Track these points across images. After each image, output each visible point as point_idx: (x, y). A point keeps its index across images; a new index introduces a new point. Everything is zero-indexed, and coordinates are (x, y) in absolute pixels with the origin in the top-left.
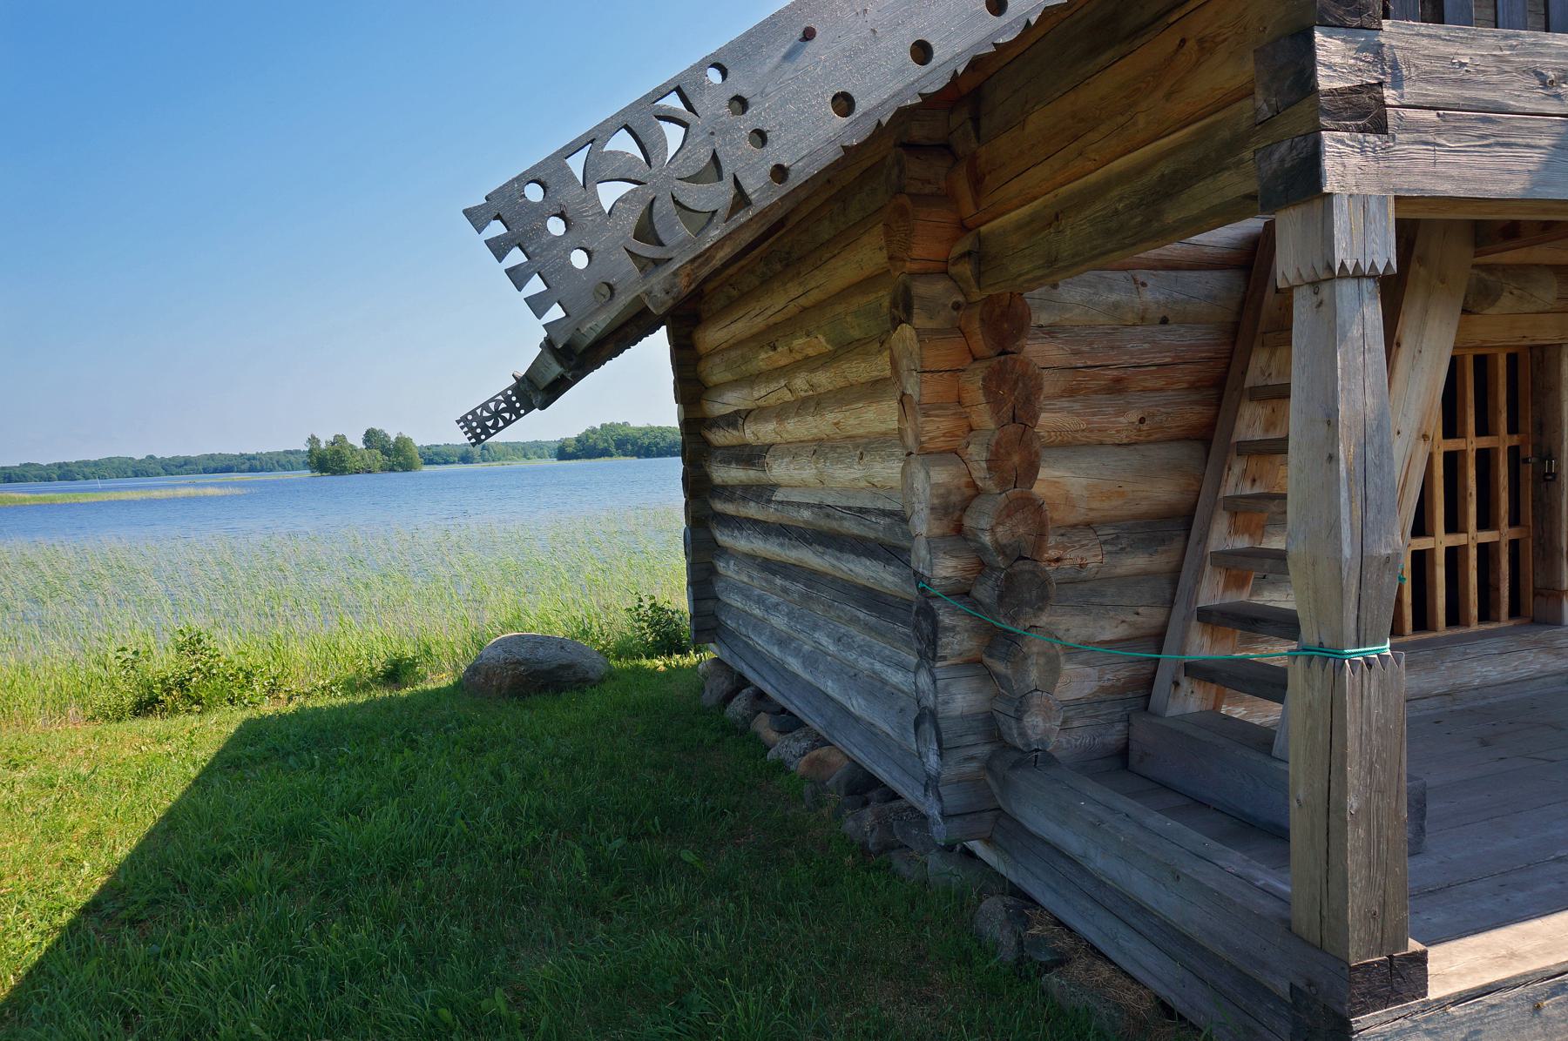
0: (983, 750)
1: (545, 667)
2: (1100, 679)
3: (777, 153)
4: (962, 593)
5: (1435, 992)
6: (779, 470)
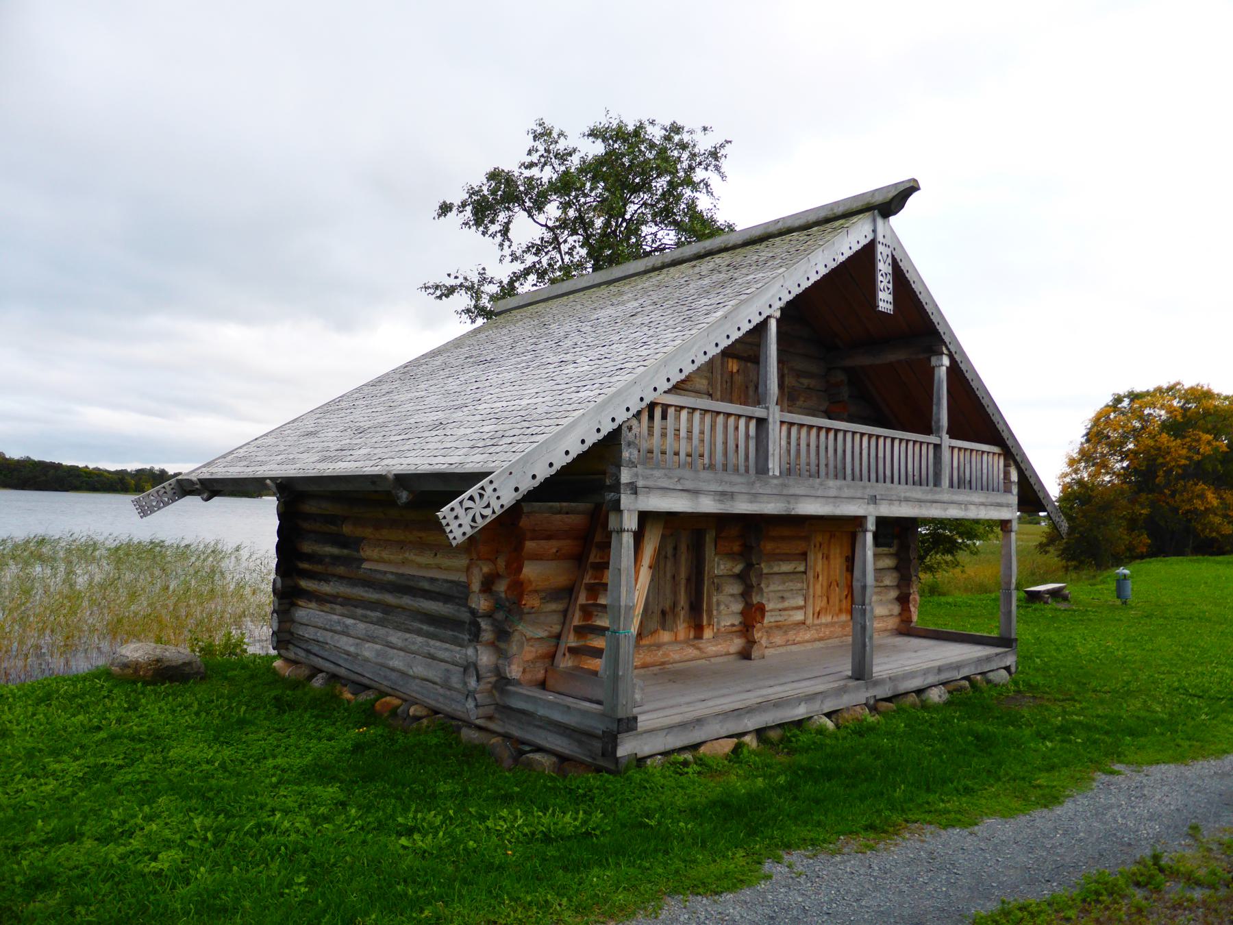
0: (493, 679)
1: (174, 664)
2: (536, 652)
3: (502, 501)
4: (489, 615)
5: (639, 729)
6: (367, 552)
